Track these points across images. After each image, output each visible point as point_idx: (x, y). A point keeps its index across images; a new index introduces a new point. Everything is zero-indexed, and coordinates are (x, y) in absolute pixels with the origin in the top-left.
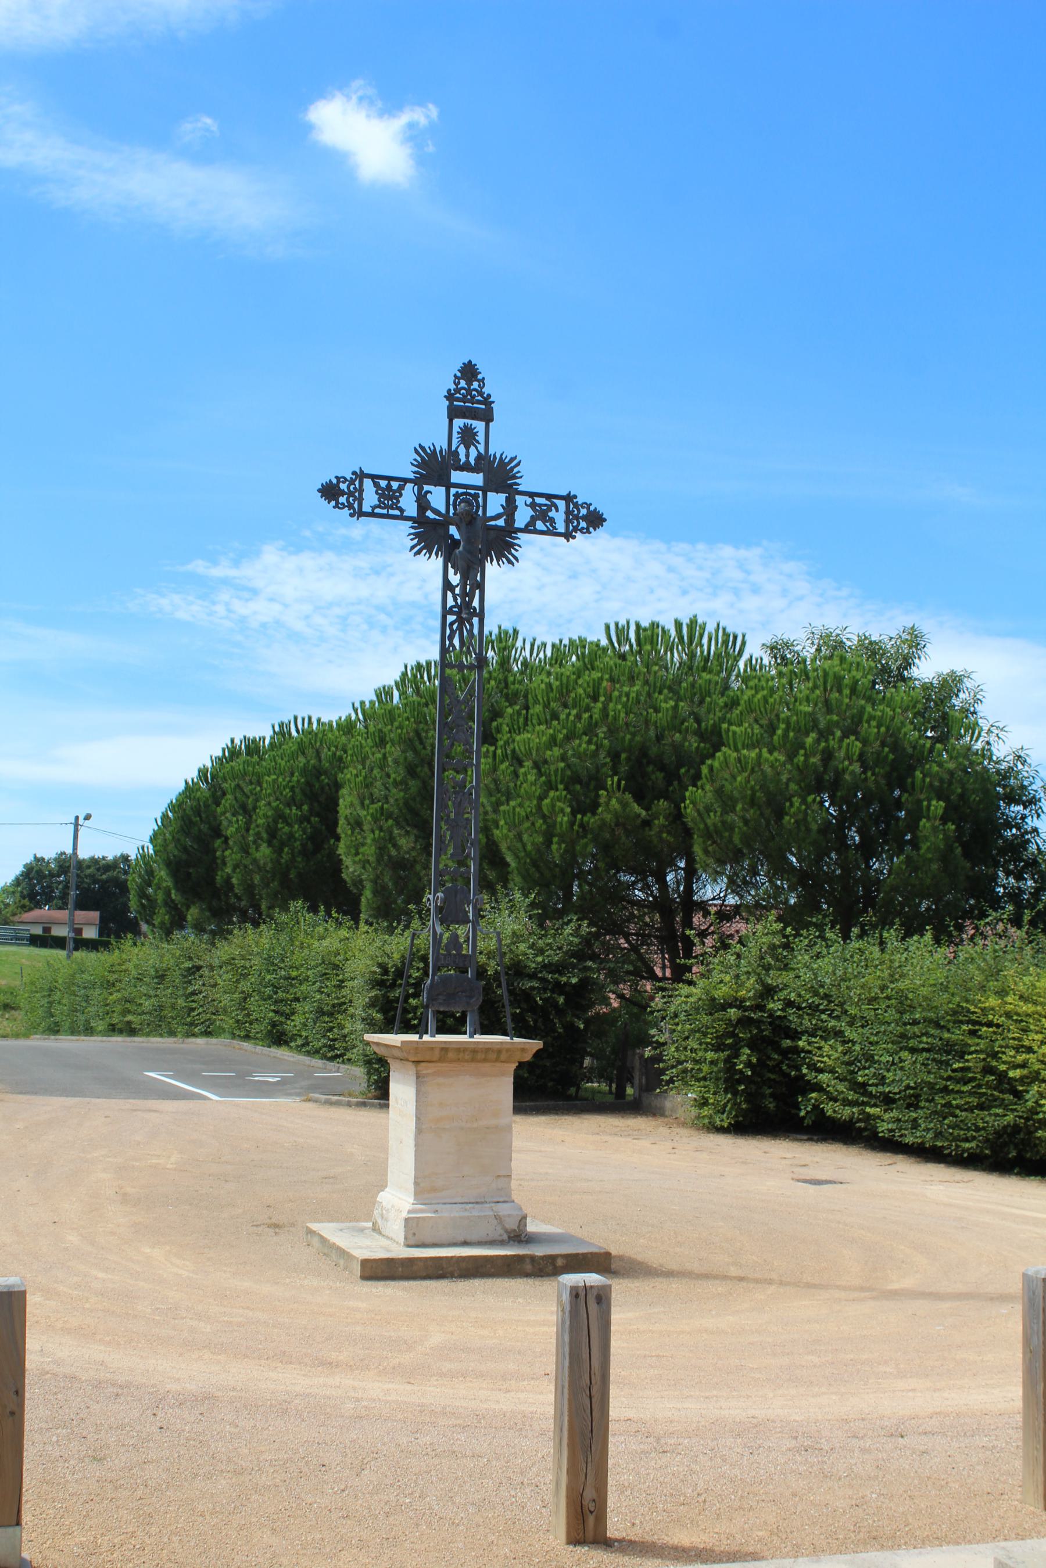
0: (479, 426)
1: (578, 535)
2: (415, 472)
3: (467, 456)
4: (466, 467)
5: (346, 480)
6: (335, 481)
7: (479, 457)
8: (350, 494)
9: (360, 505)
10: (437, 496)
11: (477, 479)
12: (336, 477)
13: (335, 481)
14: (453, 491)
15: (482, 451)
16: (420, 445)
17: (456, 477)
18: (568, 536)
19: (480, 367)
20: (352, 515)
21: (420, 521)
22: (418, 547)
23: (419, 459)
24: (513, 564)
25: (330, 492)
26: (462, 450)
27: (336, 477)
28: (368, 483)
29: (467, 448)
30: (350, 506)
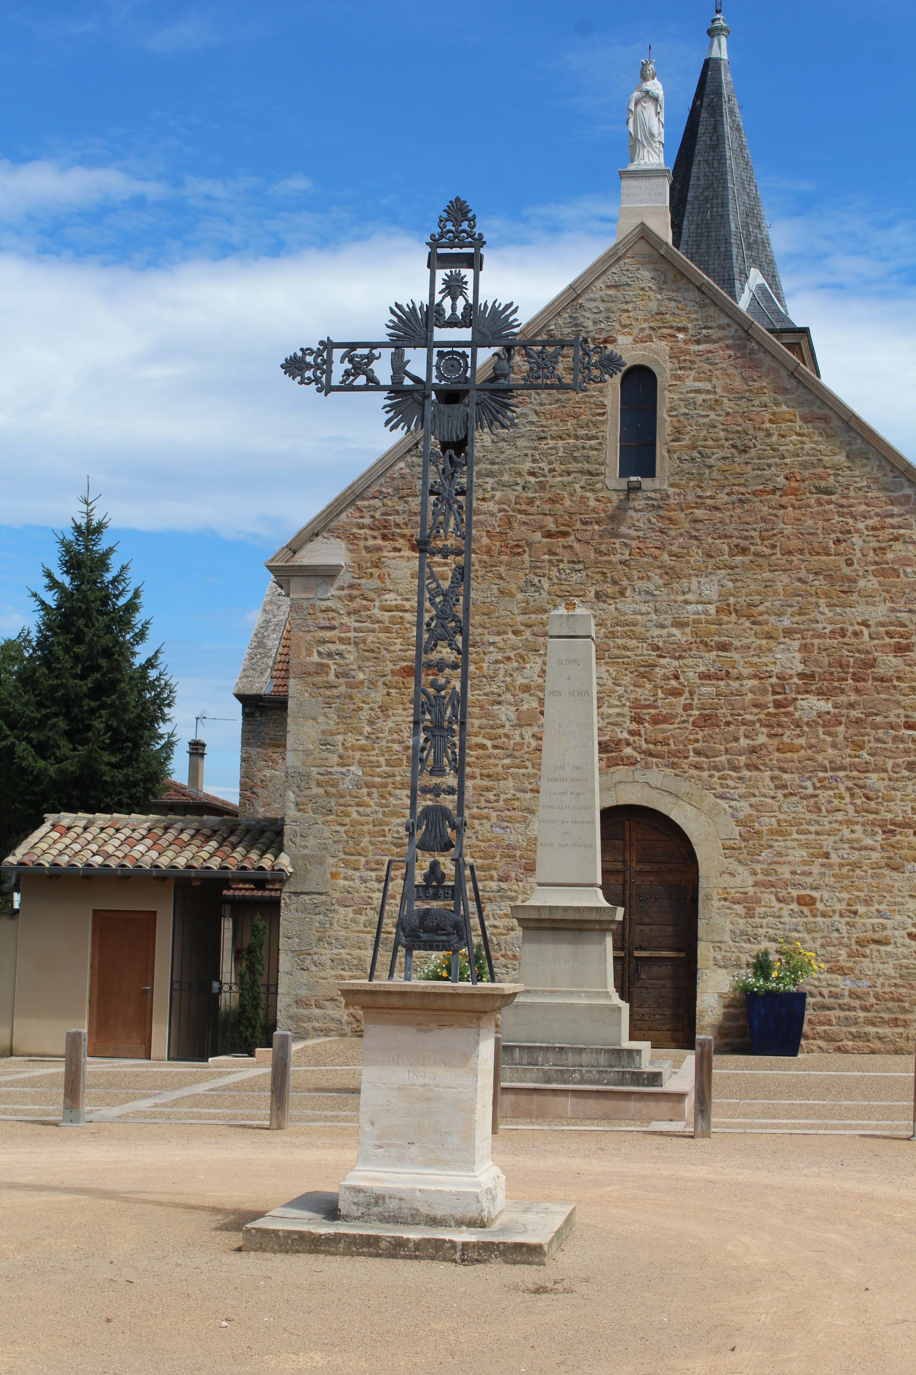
0: (468, 274)
1: (315, 347)
2: (390, 335)
3: (454, 308)
4: (452, 323)
5: (312, 352)
6: (300, 354)
7: (468, 308)
8: (317, 367)
9: (329, 379)
10: (417, 362)
11: (465, 334)
12: (302, 349)
13: (300, 354)
14: (435, 350)
15: (471, 301)
16: (396, 305)
17: (441, 334)
18: (328, 345)
19: (470, 204)
20: (319, 390)
21: (396, 390)
22: (507, 313)
23: (395, 319)
24: (396, 305)
25: (294, 366)
26: (447, 303)
27: (302, 349)
28: (338, 353)
29: (454, 299)
30: (317, 380)
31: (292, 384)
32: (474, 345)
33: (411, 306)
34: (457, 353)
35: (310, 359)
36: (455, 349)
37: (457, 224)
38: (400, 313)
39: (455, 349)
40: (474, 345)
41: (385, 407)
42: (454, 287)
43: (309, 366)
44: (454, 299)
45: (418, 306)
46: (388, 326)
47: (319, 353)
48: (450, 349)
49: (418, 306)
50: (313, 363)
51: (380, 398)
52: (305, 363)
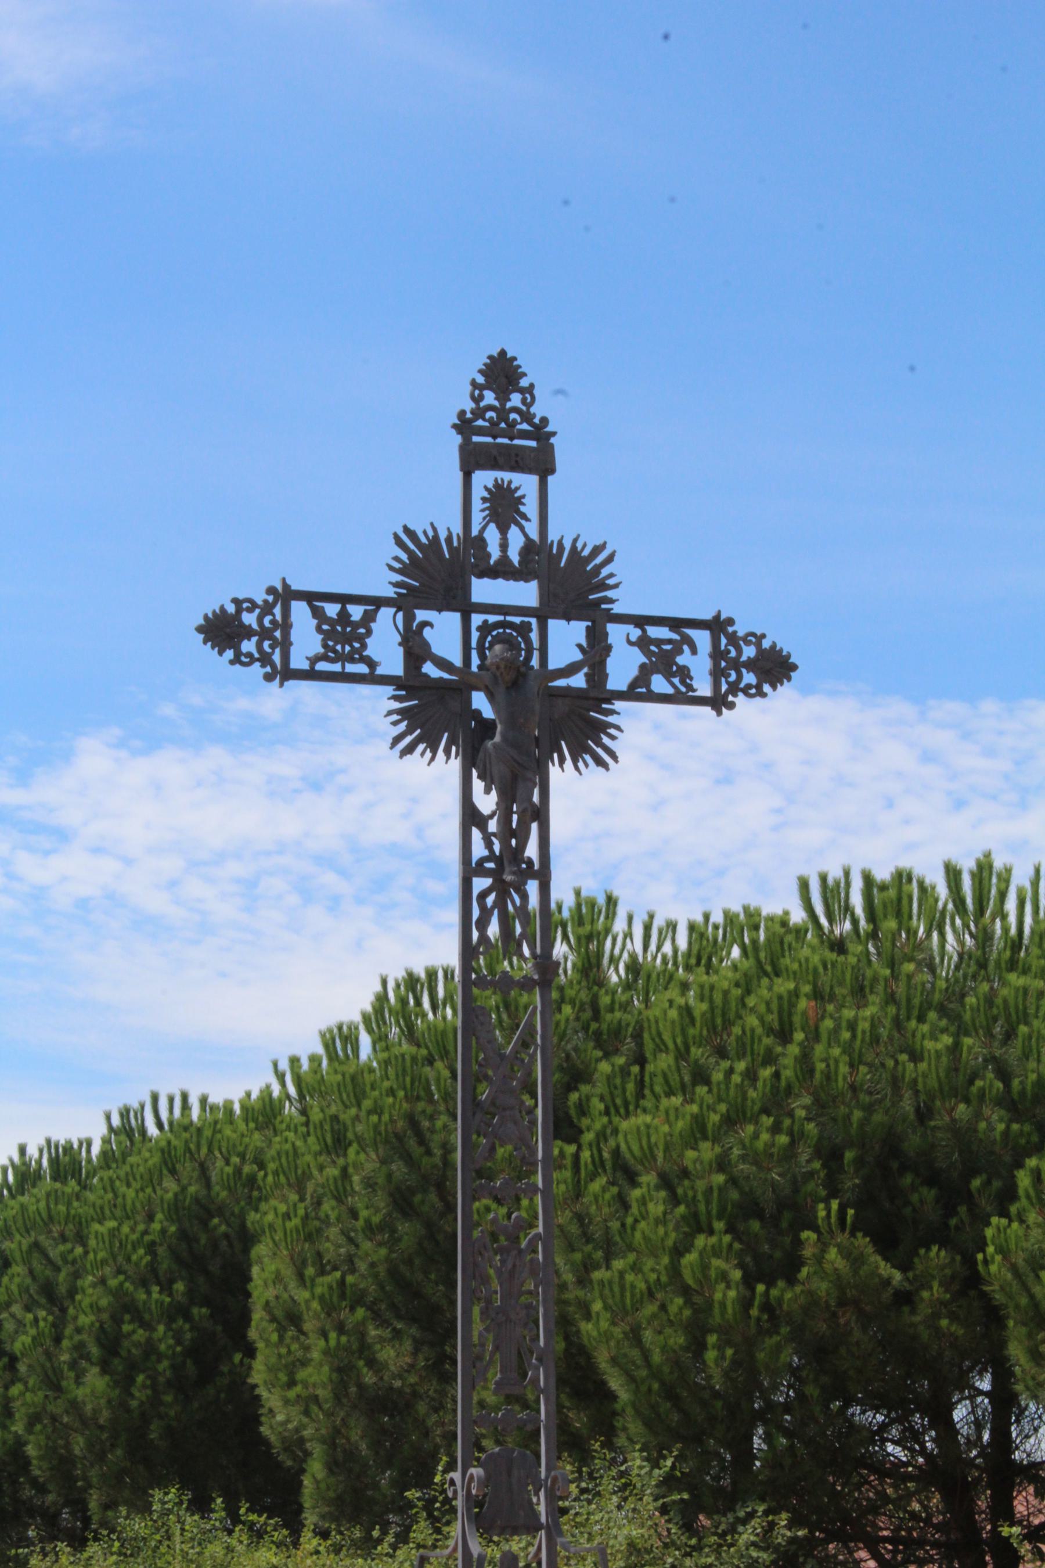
0: (526, 484)
2: (613, 712)
3: (504, 546)
4: (502, 570)
6: (231, 609)
7: (529, 549)
8: (264, 634)
9: (286, 657)
10: (444, 634)
11: (525, 594)
14: (477, 619)
15: (534, 535)
17: (484, 590)
19: (524, 363)
23: (404, 557)
25: (222, 631)
26: (492, 536)
28: (300, 610)
29: (503, 530)
30: (265, 659)
31: (778, 637)
32: (542, 615)
33: (431, 534)
34: (511, 625)
35: (249, 619)
36: (509, 618)
37: (503, 396)
38: (599, 751)
39: (509, 618)
40: (542, 615)
41: (390, 713)
42: (504, 507)
43: (247, 633)
44: (503, 530)
45: (443, 535)
46: (391, 568)
47: (267, 609)
48: (501, 618)
49: (443, 535)
50: (255, 626)
51: (624, 603)
52: (242, 625)
